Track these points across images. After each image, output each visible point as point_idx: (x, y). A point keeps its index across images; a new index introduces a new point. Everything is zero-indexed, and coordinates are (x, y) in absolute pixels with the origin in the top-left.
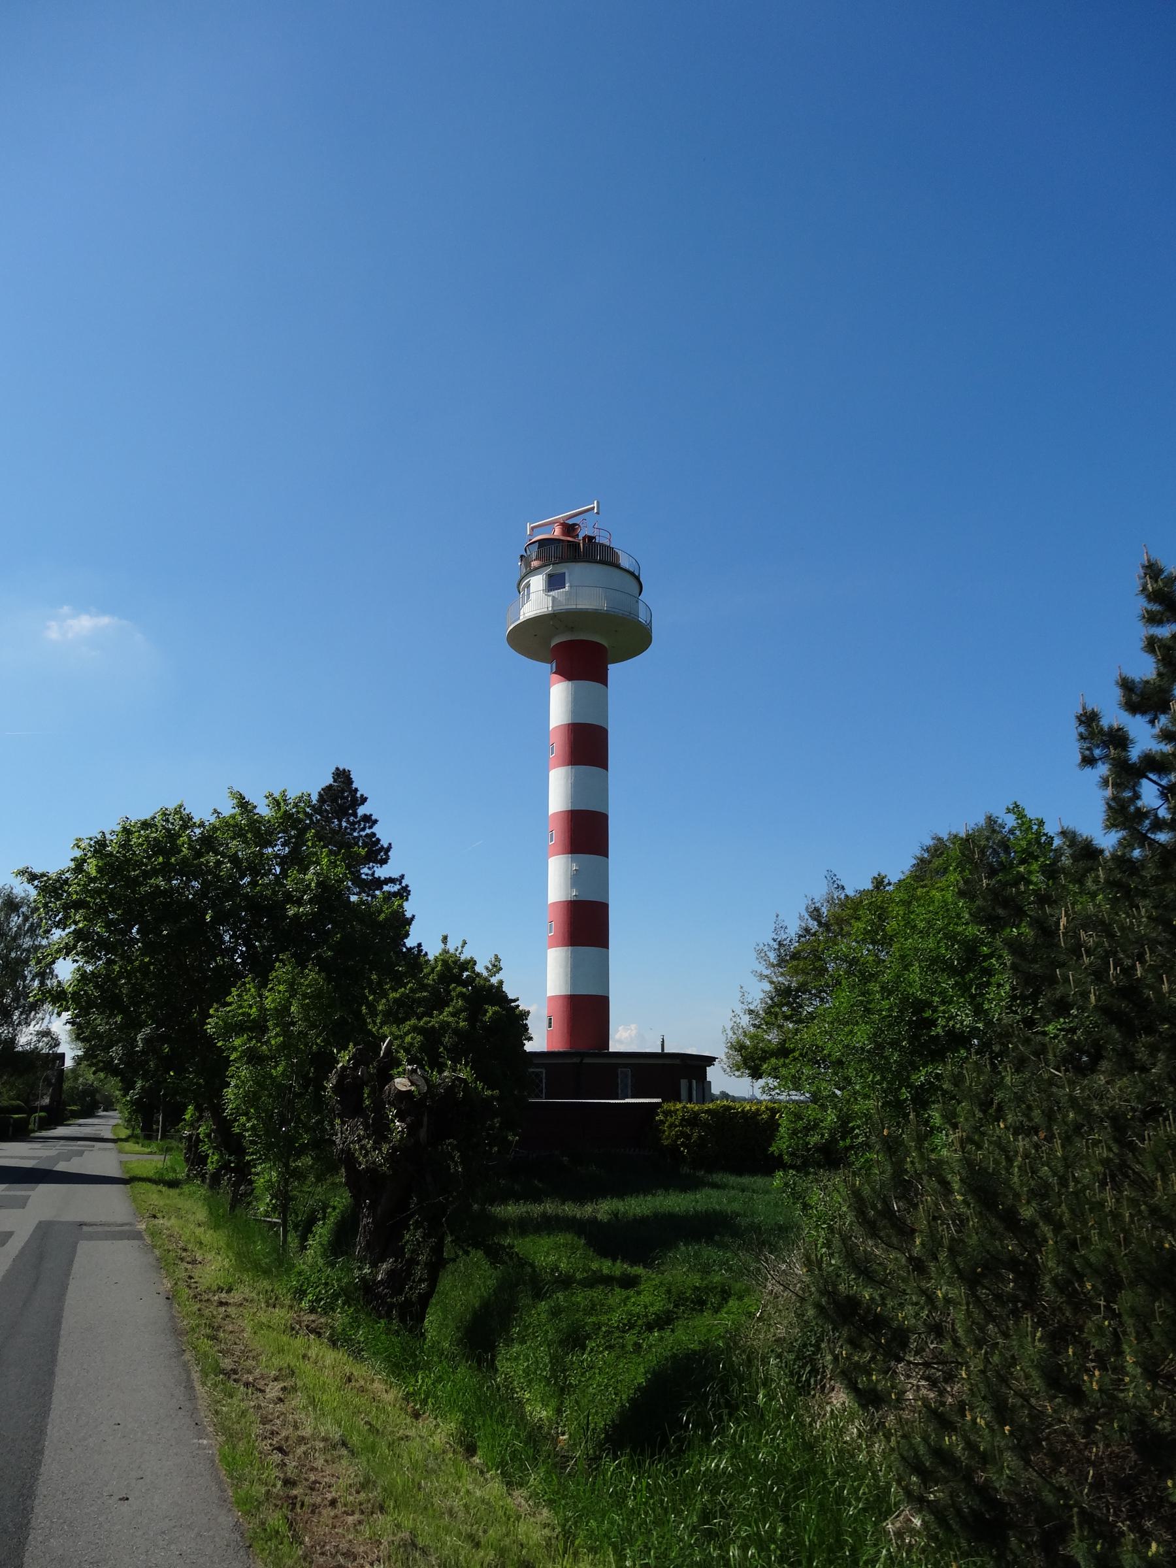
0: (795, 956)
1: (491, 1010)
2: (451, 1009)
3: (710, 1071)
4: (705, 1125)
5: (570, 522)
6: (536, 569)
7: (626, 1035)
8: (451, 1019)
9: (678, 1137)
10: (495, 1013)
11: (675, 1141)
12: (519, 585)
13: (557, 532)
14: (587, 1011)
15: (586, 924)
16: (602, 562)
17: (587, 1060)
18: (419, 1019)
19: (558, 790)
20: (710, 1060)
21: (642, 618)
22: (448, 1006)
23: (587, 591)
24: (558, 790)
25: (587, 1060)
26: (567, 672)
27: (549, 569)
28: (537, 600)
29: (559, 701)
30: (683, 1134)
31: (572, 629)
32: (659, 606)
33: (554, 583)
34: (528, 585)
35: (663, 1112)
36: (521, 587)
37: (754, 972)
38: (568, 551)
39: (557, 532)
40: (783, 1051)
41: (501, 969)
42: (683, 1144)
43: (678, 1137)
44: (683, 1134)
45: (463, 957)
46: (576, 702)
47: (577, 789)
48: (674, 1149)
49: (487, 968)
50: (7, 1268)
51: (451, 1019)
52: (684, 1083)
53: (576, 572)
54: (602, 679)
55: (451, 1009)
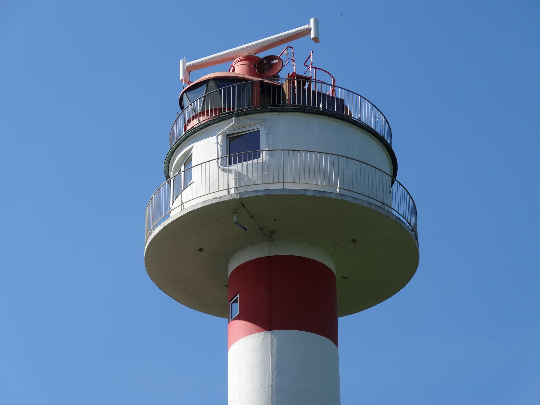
5: (262, 55)
6: (195, 131)
13: (239, 69)
16: (325, 113)
21: (399, 207)
23: (298, 161)
26: (263, 317)
27: (229, 125)
28: (208, 176)
31: (270, 235)
33: (239, 148)
34: (188, 160)
36: (172, 165)
38: (257, 96)
50: (211, 138)
53: (277, 129)
54: (331, 334)
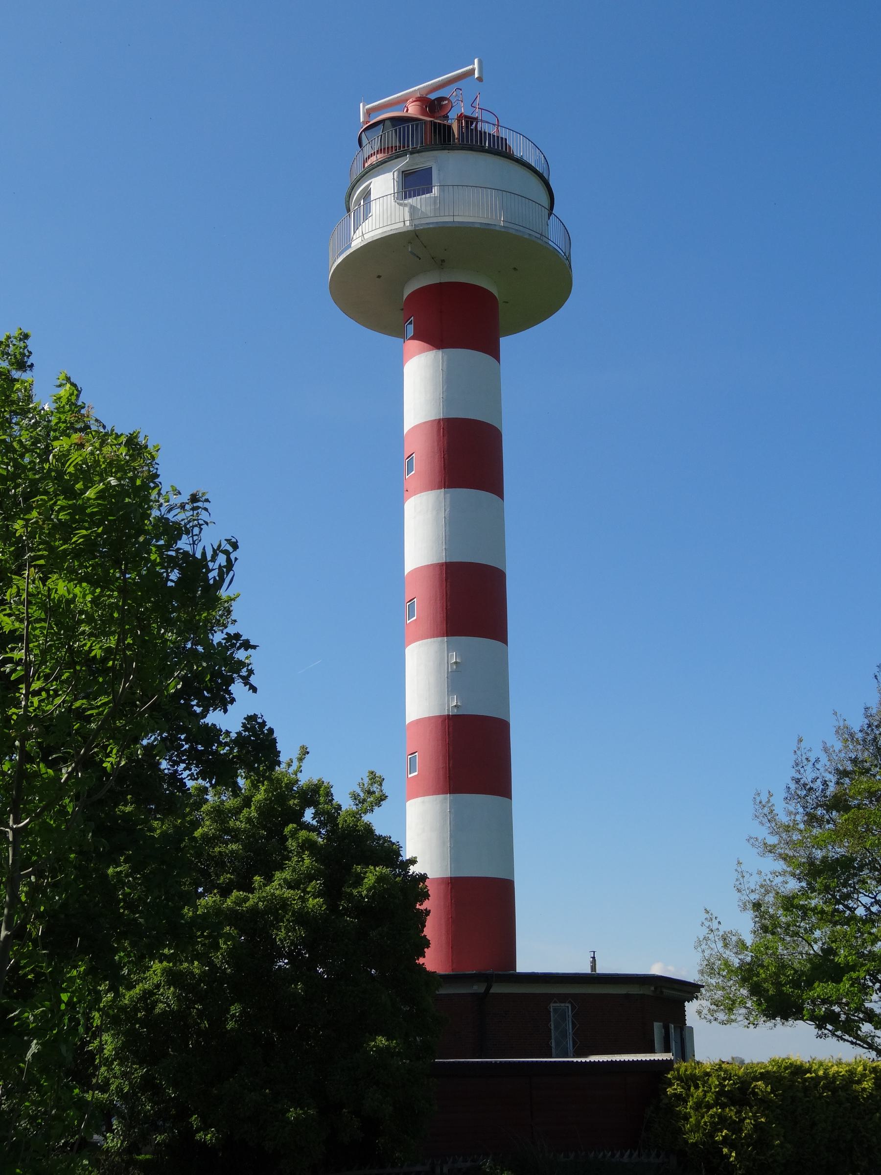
0: (838, 803)
1: (371, 875)
2: (287, 874)
3: (691, 1008)
4: (764, 1103)
5: (433, 96)
7: (544, 946)
8: (288, 893)
9: (715, 1128)
10: (381, 879)
11: (711, 1136)
12: (350, 195)
13: (413, 110)
14: (486, 903)
15: (473, 756)
17: (496, 989)
18: (225, 892)
19: (422, 529)
20: (691, 990)
22: (281, 868)
23: (466, 195)
24: (422, 529)
25: (496, 989)
26: (436, 337)
27: (404, 162)
28: (383, 210)
29: (421, 382)
30: (723, 1121)
31: (441, 264)
32: (583, 227)
33: (413, 184)
34: (367, 194)
35: (679, 1078)
36: (352, 200)
37: (751, 840)
38: (430, 134)
39: (413, 110)
40: (826, 968)
41: (383, 798)
42: (726, 1141)
43: (715, 1128)
44: (723, 1121)
45: (304, 779)
46: (451, 384)
47: (454, 527)
48: (710, 1150)
49: (355, 797)
51: (288, 893)
52: (657, 1027)
53: (446, 165)
54: (494, 351)
55: (287, 874)
